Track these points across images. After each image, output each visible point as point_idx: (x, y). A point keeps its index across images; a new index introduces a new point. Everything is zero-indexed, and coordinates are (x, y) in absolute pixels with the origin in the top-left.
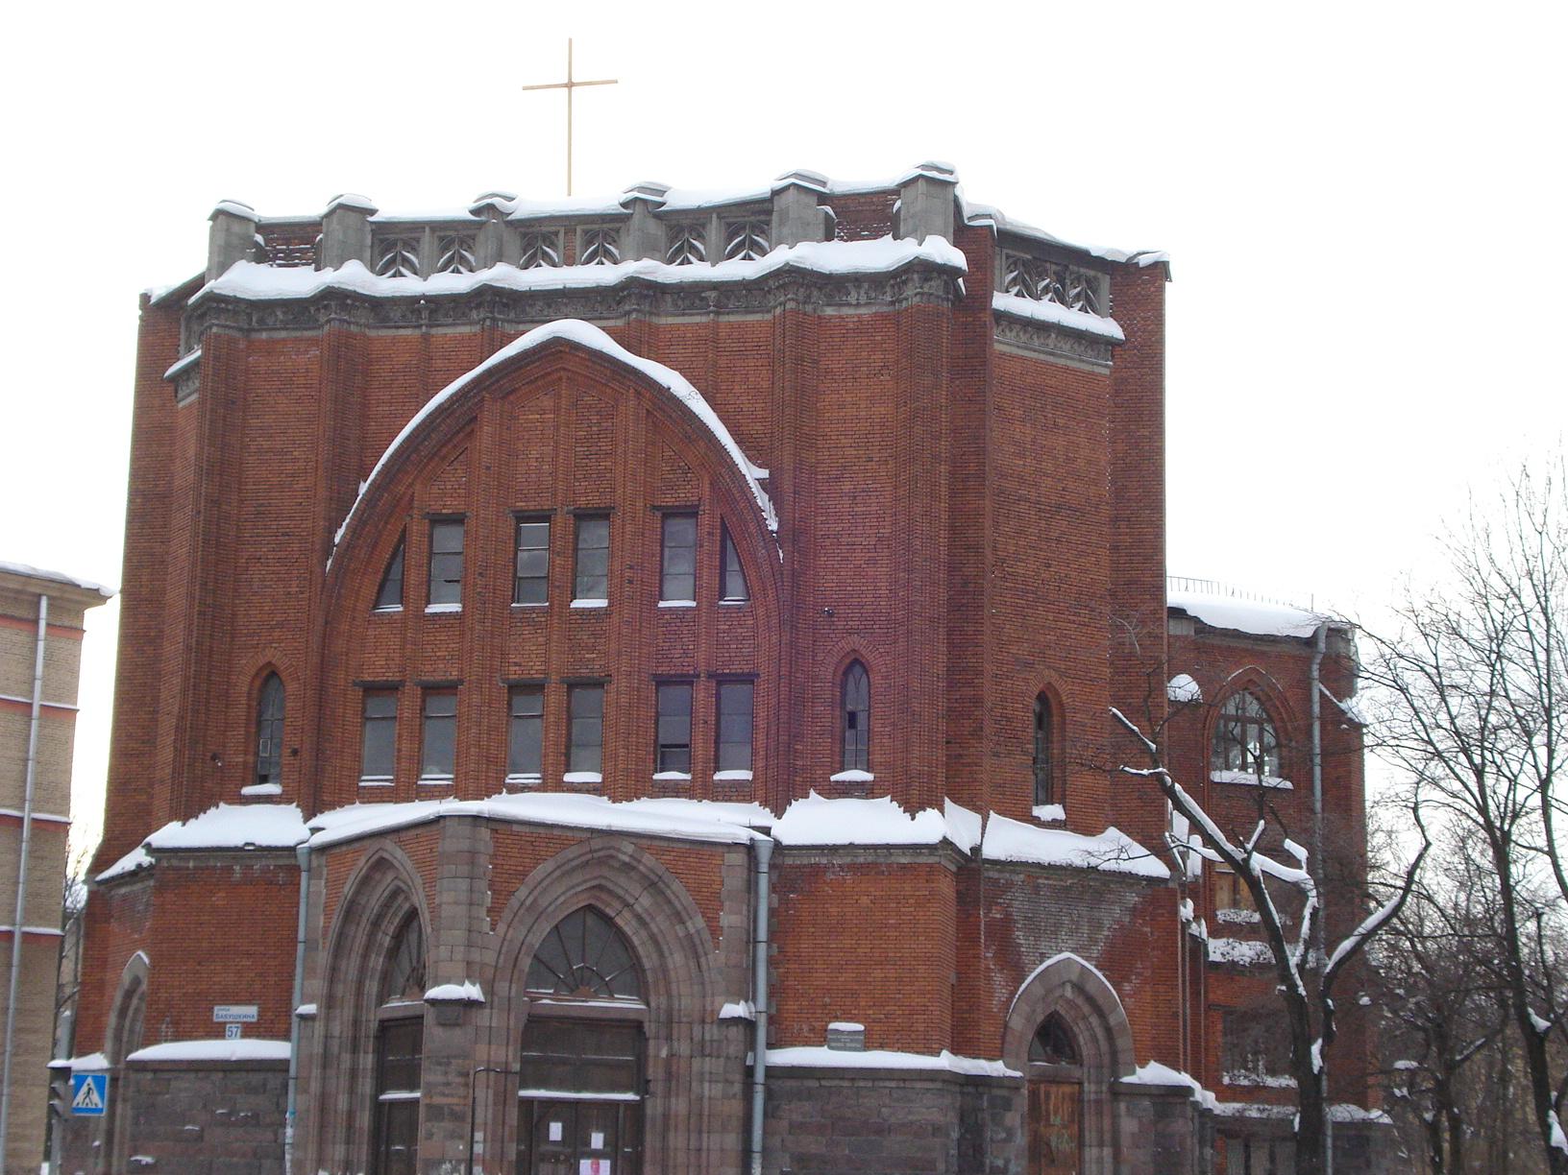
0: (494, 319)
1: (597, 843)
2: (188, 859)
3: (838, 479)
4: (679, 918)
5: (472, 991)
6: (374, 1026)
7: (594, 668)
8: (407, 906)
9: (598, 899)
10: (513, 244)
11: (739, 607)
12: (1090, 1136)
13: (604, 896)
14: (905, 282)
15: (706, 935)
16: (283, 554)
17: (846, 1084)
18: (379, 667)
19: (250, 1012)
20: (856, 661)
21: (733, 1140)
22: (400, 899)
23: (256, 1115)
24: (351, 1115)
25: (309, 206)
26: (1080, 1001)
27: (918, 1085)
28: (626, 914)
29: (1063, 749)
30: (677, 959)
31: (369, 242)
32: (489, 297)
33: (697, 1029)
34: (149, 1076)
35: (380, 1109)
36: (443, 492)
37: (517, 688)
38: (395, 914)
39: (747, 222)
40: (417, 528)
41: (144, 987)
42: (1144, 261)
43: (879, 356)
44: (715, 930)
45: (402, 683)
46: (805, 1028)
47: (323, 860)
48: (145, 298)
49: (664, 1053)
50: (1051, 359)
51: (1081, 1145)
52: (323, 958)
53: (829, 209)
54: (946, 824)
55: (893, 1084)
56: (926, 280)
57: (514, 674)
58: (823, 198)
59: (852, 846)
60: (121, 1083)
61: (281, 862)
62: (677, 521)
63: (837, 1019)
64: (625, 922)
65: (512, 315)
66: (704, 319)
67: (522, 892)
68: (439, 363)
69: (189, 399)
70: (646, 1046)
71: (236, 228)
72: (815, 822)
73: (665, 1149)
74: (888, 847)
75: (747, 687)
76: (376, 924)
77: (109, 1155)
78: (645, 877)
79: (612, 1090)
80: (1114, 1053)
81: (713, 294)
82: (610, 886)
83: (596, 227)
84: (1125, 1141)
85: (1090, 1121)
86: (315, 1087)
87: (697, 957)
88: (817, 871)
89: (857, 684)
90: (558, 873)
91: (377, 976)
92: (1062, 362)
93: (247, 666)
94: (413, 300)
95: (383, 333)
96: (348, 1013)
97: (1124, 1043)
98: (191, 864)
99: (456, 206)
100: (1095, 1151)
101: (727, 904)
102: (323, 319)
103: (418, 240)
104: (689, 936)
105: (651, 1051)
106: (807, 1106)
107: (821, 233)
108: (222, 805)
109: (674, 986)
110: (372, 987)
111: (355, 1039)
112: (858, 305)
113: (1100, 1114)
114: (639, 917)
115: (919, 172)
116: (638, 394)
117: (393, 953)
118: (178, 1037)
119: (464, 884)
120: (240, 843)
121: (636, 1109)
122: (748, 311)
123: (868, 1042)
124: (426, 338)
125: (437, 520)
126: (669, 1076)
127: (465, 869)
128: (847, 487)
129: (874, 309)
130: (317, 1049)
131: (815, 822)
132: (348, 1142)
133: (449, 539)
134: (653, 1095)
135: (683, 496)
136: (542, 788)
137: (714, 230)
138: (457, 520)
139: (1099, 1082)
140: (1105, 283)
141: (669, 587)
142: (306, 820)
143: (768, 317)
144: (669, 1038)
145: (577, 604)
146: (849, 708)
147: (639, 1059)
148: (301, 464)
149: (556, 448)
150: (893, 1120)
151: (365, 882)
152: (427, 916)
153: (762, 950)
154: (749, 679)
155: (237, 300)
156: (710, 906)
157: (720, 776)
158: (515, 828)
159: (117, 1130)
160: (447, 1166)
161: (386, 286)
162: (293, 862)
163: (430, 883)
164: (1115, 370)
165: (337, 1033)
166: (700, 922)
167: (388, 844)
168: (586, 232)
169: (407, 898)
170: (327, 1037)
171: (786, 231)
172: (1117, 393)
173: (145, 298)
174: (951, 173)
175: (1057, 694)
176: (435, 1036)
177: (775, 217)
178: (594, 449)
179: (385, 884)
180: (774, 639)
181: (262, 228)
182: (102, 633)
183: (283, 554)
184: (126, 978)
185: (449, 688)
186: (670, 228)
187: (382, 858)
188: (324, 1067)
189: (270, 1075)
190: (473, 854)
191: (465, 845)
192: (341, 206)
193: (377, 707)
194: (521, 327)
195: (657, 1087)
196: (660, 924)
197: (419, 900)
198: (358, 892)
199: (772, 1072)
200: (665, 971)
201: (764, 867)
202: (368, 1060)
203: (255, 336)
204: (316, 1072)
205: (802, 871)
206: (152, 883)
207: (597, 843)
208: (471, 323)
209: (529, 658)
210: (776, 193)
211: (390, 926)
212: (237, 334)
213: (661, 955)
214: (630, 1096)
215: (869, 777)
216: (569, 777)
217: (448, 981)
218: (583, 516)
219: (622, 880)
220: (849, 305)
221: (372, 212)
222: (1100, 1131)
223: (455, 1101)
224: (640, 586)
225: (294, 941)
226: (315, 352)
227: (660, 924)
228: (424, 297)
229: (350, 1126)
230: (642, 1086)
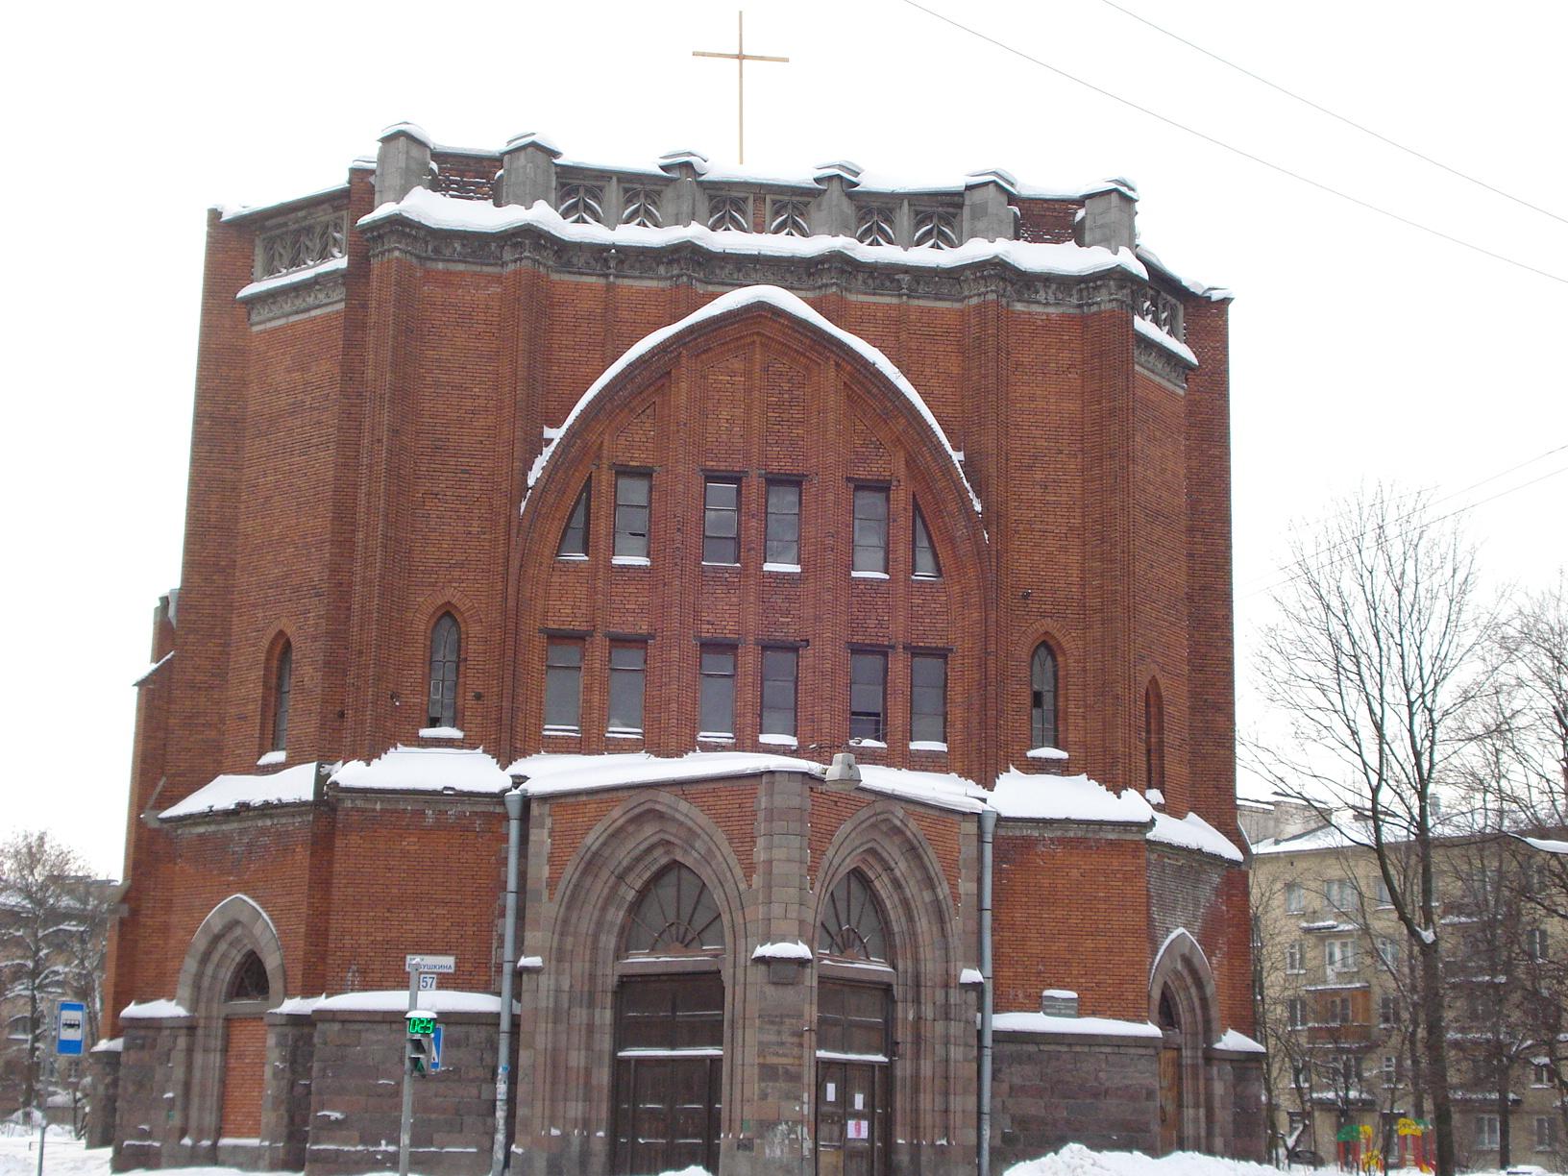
1: (879, 806)
2: (398, 801)
3: (1030, 467)
5: (801, 950)
6: (612, 982)
7: (789, 632)
10: (703, 207)
11: (932, 584)
12: (1188, 1098)
14: (1096, 288)
15: (951, 902)
16: (463, 493)
17: (1064, 1049)
18: (566, 615)
19: (447, 962)
20: (1044, 643)
23: (457, 1070)
25: (490, 141)
26: (1185, 973)
27: (1132, 1051)
30: (923, 924)
32: (689, 255)
34: (337, 1026)
35: (620, 1066)
36: (635, 443)
37: (711, 646)
39: (941, 212)
40: (605, 477)
42: (1216, 296)
43: (1066, 354)
44: (956, 897)
45: (590, 634)
47: (546, 809)
48: (215, 215)
51: (1180, 1106)
53: (1016, 209)
54: (1132, 806)
55: (1108, 1050)
57: (707, 632)
58: (1012, 199)
59: (1068, 820)
60: (200, 1032)
62: (866, 494)
63: (1051, 986)
64: (883, 887)
66: (895, 301)
68: (625, 314)
70: (894, 1010)
71: (415, 152)
72: (1021, 796)
73: (916, 1111)
74: (1101, 823)
75: (791, 656)
77: (186, 1108)
78: (908, 840)
79: (867, 1052)
80: (1207, 1021)
81: (907, 278)
83: (786, 198)
84: (1217, 1104)
85: (1188, 1084)
88: (1028, 844)
89: (1042, 665)
91: (616, 929)
92: (1157, 379)
93: (424, 604)
94: (603, 249)
95: (566, 277)
96: (581, 967)
97: (1215, 1012)
98: (378, 807)
99: (646, 161)
100: (1191, 1111)
102: (507, 256)
105: (900, 1015)
106: (1028, 1069)
107: (1012, 231)
108: (480, 750)
110: (609, 941)
111: (591, 994)
112: (1047, 304)
113: (1195, 1077)
115: (1113, 186)
118: (366, 986)
120: (439, 787)
121: (887, 1069)
123: (1082, 1009)
124: (610, 287)
125: (624, 471)
126: (918, 1039)
127: (795, 826)
129: (1060, 310)
131: (1021, 796)
132: (587, 1099)
133: (634, 492)
134: (901, 1057)
135: (874, 470)
136: (735, 748)
137: (904, 216)
138: (645, 473)
139: (1195, 1048)
141: (860, 557)
142: (504, 767)
143: (957, 305)
144: (917, 1001)
145: (768, 567)
146: (1036, 687)
147: (886, 1021)
148: (482, 402)
149: (749, 409)
150: (1108, 1084)
154: (942, 654)
155: (420, 226)
157: (915, 746)
160: (783, 1127)
161: (570, 231)
162: (499, 809)
163: (744, 842)
164: (1189, 393)
166: (945, 885)
167: (665, 797)
168: (774, 202)
171: (980, 225)
172: (1190, 413)
173: (215, 215)
174: (1132, 189)
177: (966, 211)
178: (786, 416)
179: (649, 831)
181: (438, 156)
183: (463, 493)
184: (214, 918)
185: (640, 642)
186: (859, 208)
189: (473, 1029)
191: (796, 802)
192: (534, 145)
193: (568, 654)
194: (719, 289)
195: (906, 1048)
199: (1001, 1037)
200: (914, 934)
201: (989, 838)
202: (605, 1016)
203: (429, 265)
205: (1018, 841)
207: (879, 806)
208: (660, 278)
209: (723, 617)
210: (969, 188)
214: (880, 1058)
215: (1063, 755)
216: (764, 739)
217: (783, 940)
218: (774, 481)
220: (1038, 303)
221: (555, 154)
222: (1196, 1094)
223: (790, 1061)
224: (826, 558)
226: (495, 289)
227: (912, 889)
228: (614, 246)
229: (587, 1083)
230: (890, 1047)
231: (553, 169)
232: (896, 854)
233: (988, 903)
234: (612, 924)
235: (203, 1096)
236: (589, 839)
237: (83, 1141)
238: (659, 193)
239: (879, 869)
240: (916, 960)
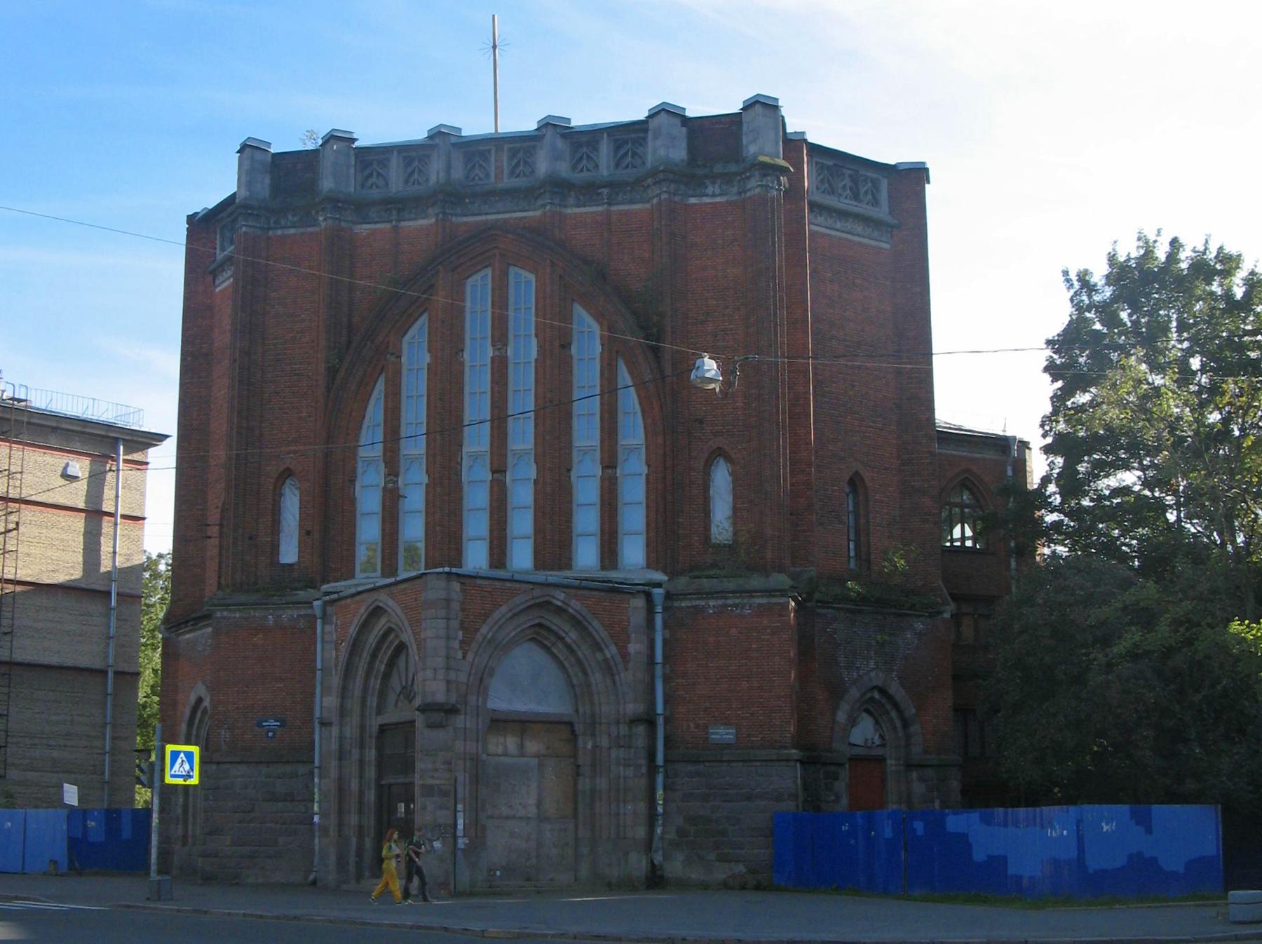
0: (444, 213)
4: (597, 646)
6: (375, 729)
8: (396, 642)
9: (538, 634)
13: (543, 632)
14: (748, 178)
15: (618, 659)
21: (642, 806)
22: (392, 636)
24: (361, 793)
28: (560, 645)
29: (868, 522)
31: (353, 162)
33: (613, 729)
38: (388, 648)
41: (206, 703)
44: (625, 655)
46: (692, 725)
49: (589, 746)
50: (849, 237)
52: (336, 680)
56: (765, 175)
58: (686, 121)
61: (302, 612)
65: (459, 211)
66: (600, 209)
67: (484, 629)
69: (225, 283)
76: (374, 656)
78: (573, 617)
81: (605, 191)
82: (548, 624)
83: (517, 145)
86: (333, 773)
87: (612, 675)
90: (509, 615)
92: (856, 239)
96: (355, 719)
101: (633, 636)
103: (388, 160)
104: (606, 660)
109: (596, 697)
110: (373, 701)
112: (714, 195)
114: (568, 647)
116: (553, 264)
117: (386, 676)
119: (442, 623)
122: (632, 202)
124: (396, 228)
128: (710, 327)
130: (334, 746)
132: (360, 812)
140: (884, 185)
143: (648, 206)
144: (593, 735)
151: (365, 626)
152: (415, 647)
153: (659, 670)
156: (621, 641)
158: (479, 582)
159: (191, 805)
165: (348, 735)
166: (614, 649)
168: (510, 149)
169: (397, 636)
170: (341, 738)
175: (862, 480)
176: (424, 736)
177: (650, 133)
180: (660, 441)
182: (163, 462)
184: (193, 699)
187: (378, 607)
188: (340, 759)
190: (448, 601)
196: (584, 651)
197: (407, 637)
198: (360, 633)
200: (589, 685)
201: (659, 609)
202: (371, 754)
203: (271, 233)
204: (334, 763)
206: (210, 630)
211: (384, 656)
212: (259, 232)
213: (585, 673)
219: (557, 620)
220: (707, 195)
221: (354, 140)
225: (314, 671)
227: (584, 651)
229: (361, 803)
231: (352, 152)
232: (567, 627)
233: (659, 658)
234: (326, 690)
235: (194, 817)
236: (351, 631)
237: (1012, 870)
238: (428, 157)
239: (553, 638)
240: (592, 703)
